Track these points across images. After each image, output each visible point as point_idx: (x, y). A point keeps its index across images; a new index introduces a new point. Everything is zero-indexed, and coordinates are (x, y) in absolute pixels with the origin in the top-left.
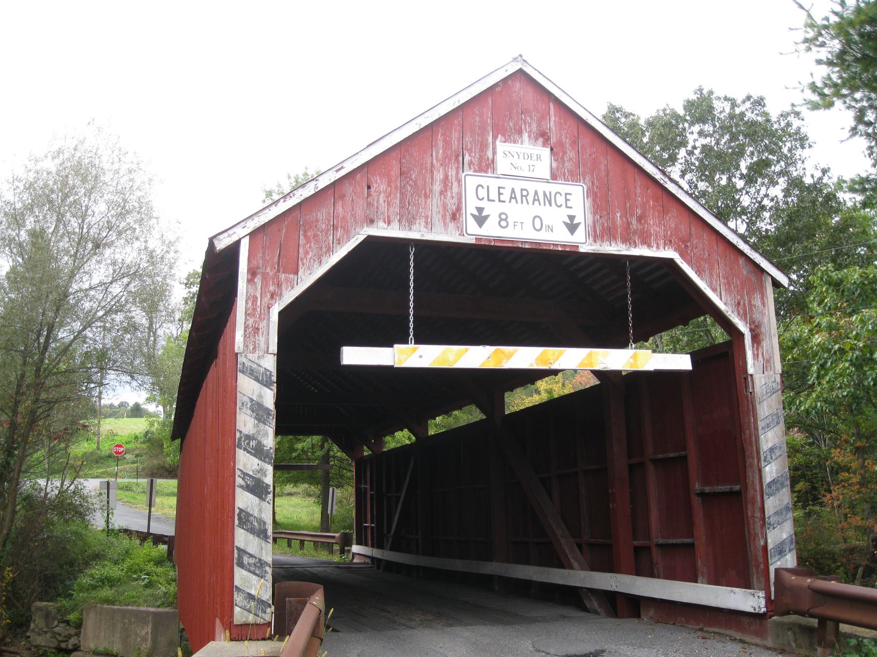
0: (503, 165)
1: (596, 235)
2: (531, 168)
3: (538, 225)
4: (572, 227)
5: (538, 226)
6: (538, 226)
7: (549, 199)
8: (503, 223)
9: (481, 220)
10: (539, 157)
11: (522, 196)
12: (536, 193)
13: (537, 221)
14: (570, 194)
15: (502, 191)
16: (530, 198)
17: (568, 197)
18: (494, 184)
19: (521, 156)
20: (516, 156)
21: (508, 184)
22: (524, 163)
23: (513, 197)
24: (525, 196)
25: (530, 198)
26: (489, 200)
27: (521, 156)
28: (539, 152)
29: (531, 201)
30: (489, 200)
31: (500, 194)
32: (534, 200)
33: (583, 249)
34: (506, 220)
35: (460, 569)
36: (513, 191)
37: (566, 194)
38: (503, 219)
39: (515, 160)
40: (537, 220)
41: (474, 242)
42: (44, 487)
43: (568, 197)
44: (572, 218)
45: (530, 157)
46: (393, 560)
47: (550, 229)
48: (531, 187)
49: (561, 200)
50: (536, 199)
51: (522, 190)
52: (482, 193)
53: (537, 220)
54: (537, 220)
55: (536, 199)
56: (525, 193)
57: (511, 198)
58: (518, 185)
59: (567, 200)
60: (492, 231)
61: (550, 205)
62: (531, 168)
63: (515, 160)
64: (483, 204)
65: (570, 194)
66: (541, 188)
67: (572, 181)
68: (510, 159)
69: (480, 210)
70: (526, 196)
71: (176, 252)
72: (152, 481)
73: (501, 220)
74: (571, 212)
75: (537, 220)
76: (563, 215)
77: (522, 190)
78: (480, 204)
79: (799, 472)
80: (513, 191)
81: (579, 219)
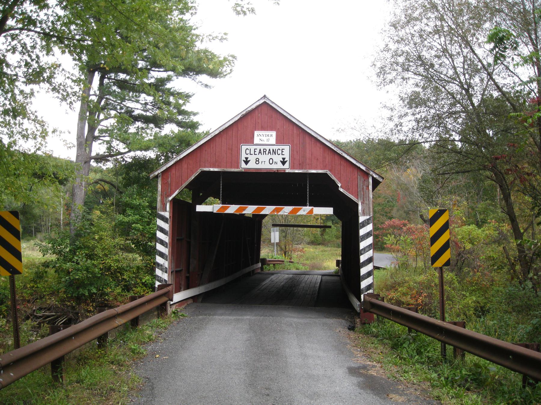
0: (256, 140)
1: (292, 166)
3: (271, 162)
4: (283, 162)
5: (271, 162)
6: (271, 162)
7: (274, 152)
8: (257, 162)
9: (247, 162)
10: (271, 135)
11: (264, 152)
12: (270, 150)
15: (256, 150)
16: (267, 152)
17: (283, 150)
18: (252, 148)
19: (264, 136)
20: (262, 135)
21: (258, 148)
22: (265, 138)
23: (260, 152)
25: (267, 152)
26: (250, 154)
27: (264, 136)
28: (271, 133)
29: (267, 154)
30: (250, 154)
31: (255, 151)
32: (269, 153)
33: (287, 171)
34: (258, 161)
35: (160, 198)
36: (260, 150)
38: (257, 160)
39: (262, 138)
40: (271, 160)
41: (243, 171)
42: (7, 292)
43: (283, 150)
45: (268, 135)
46: (213, 288)
47: (276, 163)
48: (267, 148)
49: (280, 152)
50: (269, 152)
51: (264, 149)
52: (248, 152)
53: (271, 160)
54: (271, 160)
57: (259, 153)
58: (262, 148)
60: (252, 165)
61: (275, 154)
63: (262, 138)
64: (248, 156)
66: (271, 148)
68: (260, 137)
69: (247, 158)
70: (265, 152)
71: (58, 73)
72: (534, 80)
73: (256, 161)
74: (283, 157)
75: (271, 160)
76: (280, 158)
77: (264, 149)
78: (247, 156)
79: (464, 293)
80: (260, 150)
81: (287, 159)
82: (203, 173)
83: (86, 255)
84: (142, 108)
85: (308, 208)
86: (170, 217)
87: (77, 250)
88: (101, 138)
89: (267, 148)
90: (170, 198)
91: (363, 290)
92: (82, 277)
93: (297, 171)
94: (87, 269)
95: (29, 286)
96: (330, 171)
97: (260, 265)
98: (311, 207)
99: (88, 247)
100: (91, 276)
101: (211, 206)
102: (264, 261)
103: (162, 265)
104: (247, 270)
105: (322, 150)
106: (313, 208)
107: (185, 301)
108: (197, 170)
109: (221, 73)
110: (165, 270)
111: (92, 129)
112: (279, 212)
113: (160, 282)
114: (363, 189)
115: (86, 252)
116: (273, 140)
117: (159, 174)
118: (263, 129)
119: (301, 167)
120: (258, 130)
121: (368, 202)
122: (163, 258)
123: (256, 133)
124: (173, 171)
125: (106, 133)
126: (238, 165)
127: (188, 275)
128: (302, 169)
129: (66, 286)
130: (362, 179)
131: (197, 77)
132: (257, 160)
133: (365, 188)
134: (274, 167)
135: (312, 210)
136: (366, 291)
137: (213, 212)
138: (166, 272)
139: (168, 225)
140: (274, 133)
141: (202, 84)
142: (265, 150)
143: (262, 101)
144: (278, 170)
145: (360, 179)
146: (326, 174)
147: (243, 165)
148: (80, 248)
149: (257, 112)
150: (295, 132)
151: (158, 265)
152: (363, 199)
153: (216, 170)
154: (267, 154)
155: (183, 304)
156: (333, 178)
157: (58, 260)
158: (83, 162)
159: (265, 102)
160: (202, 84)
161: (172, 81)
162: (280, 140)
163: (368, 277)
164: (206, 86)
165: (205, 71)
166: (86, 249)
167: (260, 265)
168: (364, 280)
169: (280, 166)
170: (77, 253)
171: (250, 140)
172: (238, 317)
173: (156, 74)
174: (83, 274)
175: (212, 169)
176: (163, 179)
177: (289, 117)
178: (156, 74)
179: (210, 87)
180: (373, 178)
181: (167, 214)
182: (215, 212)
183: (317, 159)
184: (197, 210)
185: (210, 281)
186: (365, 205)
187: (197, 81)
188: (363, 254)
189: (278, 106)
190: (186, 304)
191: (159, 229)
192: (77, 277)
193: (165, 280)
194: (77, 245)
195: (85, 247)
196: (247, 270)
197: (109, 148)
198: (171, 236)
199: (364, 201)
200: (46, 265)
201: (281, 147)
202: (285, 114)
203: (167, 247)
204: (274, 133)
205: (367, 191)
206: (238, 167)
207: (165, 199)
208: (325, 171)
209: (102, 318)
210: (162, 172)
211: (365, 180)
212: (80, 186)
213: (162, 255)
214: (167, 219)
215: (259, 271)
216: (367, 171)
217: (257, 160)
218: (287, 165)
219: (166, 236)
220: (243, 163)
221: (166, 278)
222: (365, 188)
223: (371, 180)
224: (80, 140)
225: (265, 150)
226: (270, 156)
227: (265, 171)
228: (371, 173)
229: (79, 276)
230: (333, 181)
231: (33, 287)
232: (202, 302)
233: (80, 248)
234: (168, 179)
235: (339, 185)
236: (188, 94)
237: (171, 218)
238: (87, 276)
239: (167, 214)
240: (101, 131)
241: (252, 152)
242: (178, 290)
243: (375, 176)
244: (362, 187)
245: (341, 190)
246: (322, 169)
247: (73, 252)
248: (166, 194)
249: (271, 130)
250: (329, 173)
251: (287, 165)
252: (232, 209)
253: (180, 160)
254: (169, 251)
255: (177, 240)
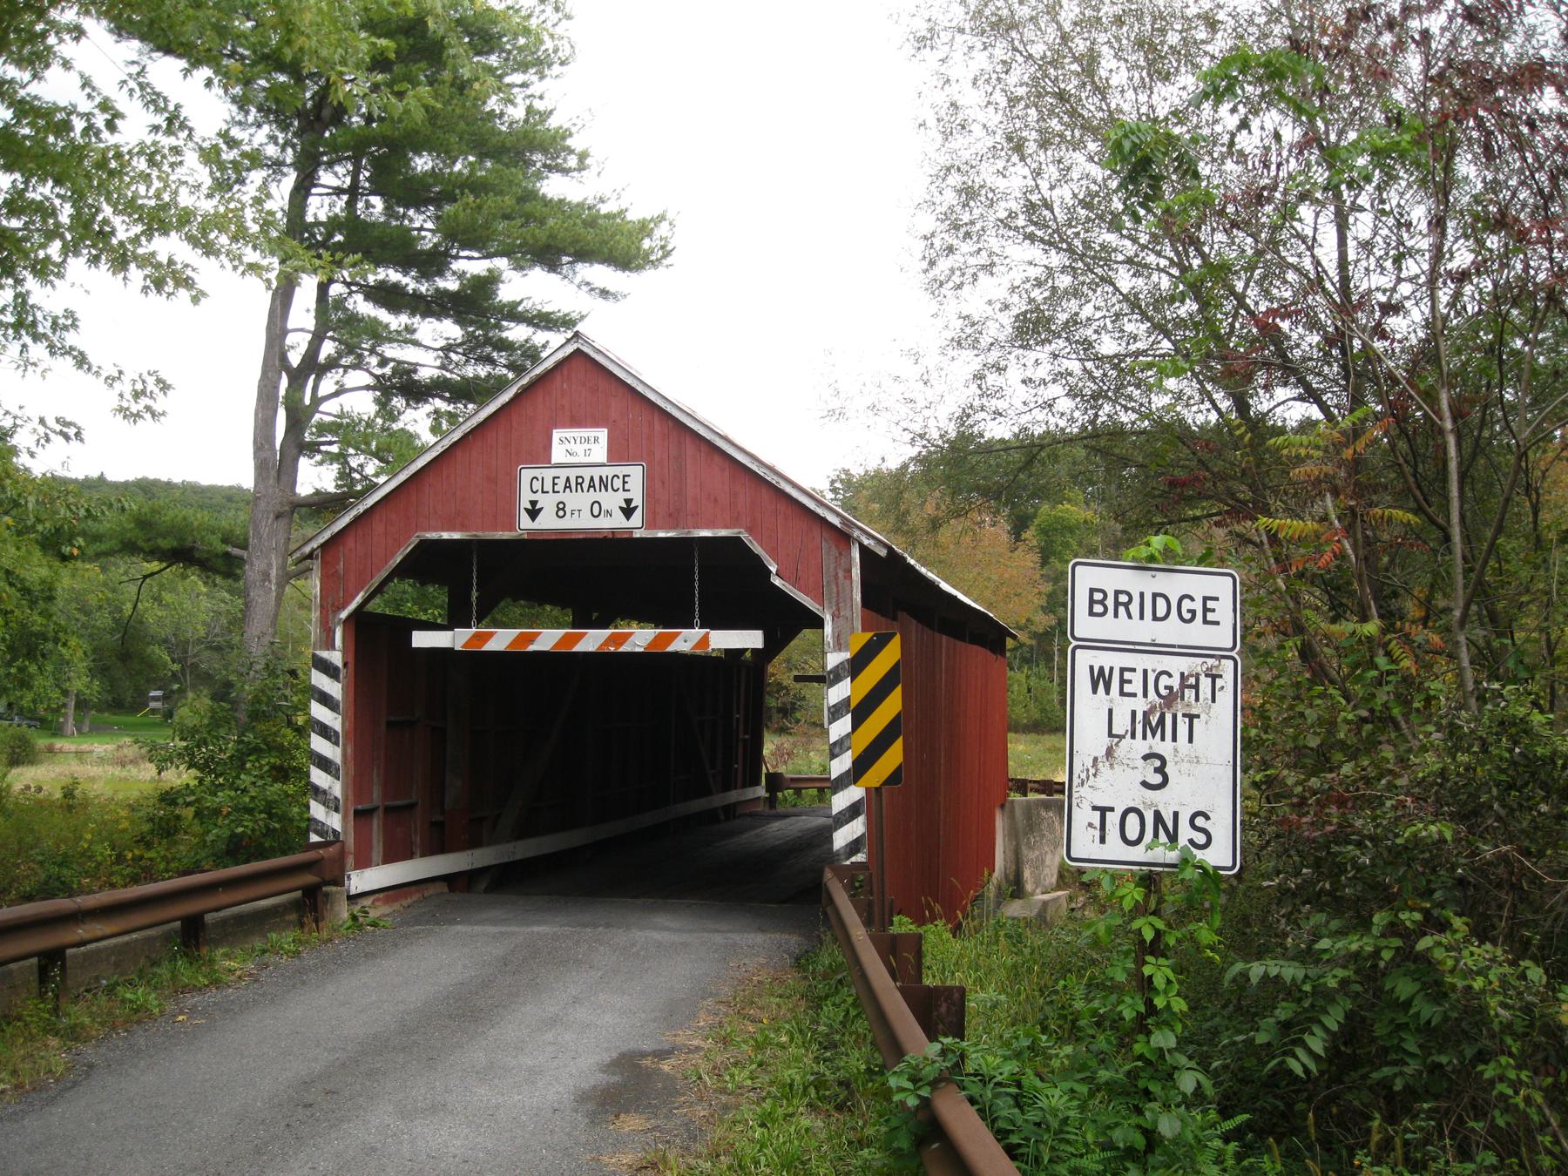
0: (558, 454)
1: (650, 522)
2: (587, 452)
4: (628, 511)
5: (596, 512)
6: (596, 512)
8: (561, 513)
9: (534, 513)
10: (596, 440)
11: (1117, 604)
12: (592, 478)
13: (596, 509)
14: (1216, 599)
18: (548, 474)
21: (563, 473)
22: (579, 448)
23: (567, 486)
24: (1123, 604)
29: (585, 489)
31: (554, 484)
33: (637, 534)
34: (563, 509)
36: (568, 479)
37: (1205, 599)
38: (561, 508)
39: (571, 446)
41: (526, 537)
44: (628, 501)
45: (587, 440)
46: (531, 854)
49: (618, 483)
50: (592, 485)
53: (596, 505)
55: (592, 485)
56: (1123, 598)
59: (624, 482)
60: (547, 521)
62: (587, 452)
65: (1216, 599)
66: (597, 473)
67: (1165, 562)
70: (1126, 605)
73: (559, 509)
74: (628, 495)
75: (596, 505)
78: (534, 497)
80: (568, 479)
82: (424, 545)
83: (273, 767)
84: (438, 363)
85: (696, 633)
86: (345, 665)
87: (249, 755)
88: (323, 448)
89: (587, 473)
90: (344, 615)
91: (838, 853)
92: (253, 830)
93: (661, 534)
94: (269, 809)
95: (130, 856)
96: (750, 530)
97: (761, 791)
98: (704, 631)
99: (281, 749)
100: (277, 826)
101: (449, 634)
102: (775, 782)
103: (325, 792)
104: (719, 800)
105: (727, 473)
106: (708, 633)
107: (413, 888)
108: (410, 537)
109: (636, 257)
110: (333, 805)
111: (297, 420)
112: (621, 644)
113: (322, 837)
114: (836, 576)
115: (272, 760)
116: (600, 453)
117: (313, 550)
118: (575, 422)
119: (673, 520)
120: (563, 426)
121: (848, 614)
122: (329, 773)
123: (557, 434)
124: (350, 542)
125: (335, 433)
126: (511, 523)
127: (438, 818)
128: (674, 527)
129: (213, 855)
130: (834, 551)
131: (579, 266)
132: (561, 506)
133: (841, 574)
134: (604, 523)
135: (706, 637)
136: (848, 858)
137: (451, 650)
138: (337, 810)
139: (340, 686)
140: (603, 434)
141: (592, 290)
142: (580, 480)
143: (570, 349)
144: (613, 531)
145: (828, 550)
146: (737, 541)
147: (525, 522)
148: (256, 750)
149: (558, 377)
150: (657, 427)
151: (318, 792)
152: (837, 604)
153: (456, 536)
154: (585, 489)
155: (396, 899)
156: (757, 549)
157: (201, 781)
158: (272, 516)
159: (578, 350)
160: (592, 290)
161: (502, 282)
162: (618, 453)
163: (852, 818)
164: (604, 293)
165: (593, 252)
166: (274, 754)
167: (761, 791)
168: (842, 826)
169: (617, 521)
170: (248, 765)
171: (541, 455)
172: (503, 929)
173: (471, 265)
174: (256, 822)
175: (446, 535)
176: (324, 564)
177: (640, 388)
178: (471, 265)
179: (615, 296)
180: (863, 549)
181: (336, 658)
182: (458, 648)
183: (716, 500)
184: (414, 645)
185: (522, 833)
186: (841, 621)
187: (577, 280)
188: (837, 756)
189: (612, 361)
190: (415, 897)
191: (316, 696)
192: (240, 830)
193: (334, 831)
194: (249, 743)
195: (270, 749)
196: (719, 800)
197: (345, 475)
198: (351, 714)
199: (838, 609)
200: (169, 798)
201: (621, 471)
202: (629, 381)
203: (336, 743)
204: (603, 434)
205: (848, 582)
206: (512, 528)
207: (331, 617)
208: (736, 530)
209: (9, 920)
210: (322, 546)
211: (840, 554)
212: (264, 581)
213: (324, 764)
214: (336, 669)
215: (760, 808)
216: (845, 529)
217: (561, 508)
218: (637, 519)
219: (335, 715)
220: (524, 513)
221: (338, 827)
222: (841, 574)
223: (856, 554)
224: (263, 455)
225: (580, 480)
226: (593, 496)
227: (581, 536)
228: (856, 533)
229: (246, 827)
230: (758, 557)
231: (141, 858)
232: (487, 891)
233: (256, 750)
234: (338, 563)
235: (773, 569)
236: (566, 315)
237: (351, 666)
238: (267, 827)
239: (336, 658)
240: (323, 428)
241: (548, 486)
242: (363, 863)
243: (866, 542)
244: (833, 573)
245: (777, 582)
246: (726, 527)
247: (239, 761)
248: (333, 605)
249: (596, 424)
250: (745, 536)
251: (637, 519)
252: (592, 640)
253: (366, 512)
254: (344, 755)
255: (389, 724)
